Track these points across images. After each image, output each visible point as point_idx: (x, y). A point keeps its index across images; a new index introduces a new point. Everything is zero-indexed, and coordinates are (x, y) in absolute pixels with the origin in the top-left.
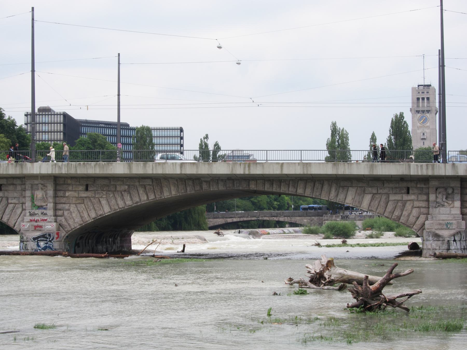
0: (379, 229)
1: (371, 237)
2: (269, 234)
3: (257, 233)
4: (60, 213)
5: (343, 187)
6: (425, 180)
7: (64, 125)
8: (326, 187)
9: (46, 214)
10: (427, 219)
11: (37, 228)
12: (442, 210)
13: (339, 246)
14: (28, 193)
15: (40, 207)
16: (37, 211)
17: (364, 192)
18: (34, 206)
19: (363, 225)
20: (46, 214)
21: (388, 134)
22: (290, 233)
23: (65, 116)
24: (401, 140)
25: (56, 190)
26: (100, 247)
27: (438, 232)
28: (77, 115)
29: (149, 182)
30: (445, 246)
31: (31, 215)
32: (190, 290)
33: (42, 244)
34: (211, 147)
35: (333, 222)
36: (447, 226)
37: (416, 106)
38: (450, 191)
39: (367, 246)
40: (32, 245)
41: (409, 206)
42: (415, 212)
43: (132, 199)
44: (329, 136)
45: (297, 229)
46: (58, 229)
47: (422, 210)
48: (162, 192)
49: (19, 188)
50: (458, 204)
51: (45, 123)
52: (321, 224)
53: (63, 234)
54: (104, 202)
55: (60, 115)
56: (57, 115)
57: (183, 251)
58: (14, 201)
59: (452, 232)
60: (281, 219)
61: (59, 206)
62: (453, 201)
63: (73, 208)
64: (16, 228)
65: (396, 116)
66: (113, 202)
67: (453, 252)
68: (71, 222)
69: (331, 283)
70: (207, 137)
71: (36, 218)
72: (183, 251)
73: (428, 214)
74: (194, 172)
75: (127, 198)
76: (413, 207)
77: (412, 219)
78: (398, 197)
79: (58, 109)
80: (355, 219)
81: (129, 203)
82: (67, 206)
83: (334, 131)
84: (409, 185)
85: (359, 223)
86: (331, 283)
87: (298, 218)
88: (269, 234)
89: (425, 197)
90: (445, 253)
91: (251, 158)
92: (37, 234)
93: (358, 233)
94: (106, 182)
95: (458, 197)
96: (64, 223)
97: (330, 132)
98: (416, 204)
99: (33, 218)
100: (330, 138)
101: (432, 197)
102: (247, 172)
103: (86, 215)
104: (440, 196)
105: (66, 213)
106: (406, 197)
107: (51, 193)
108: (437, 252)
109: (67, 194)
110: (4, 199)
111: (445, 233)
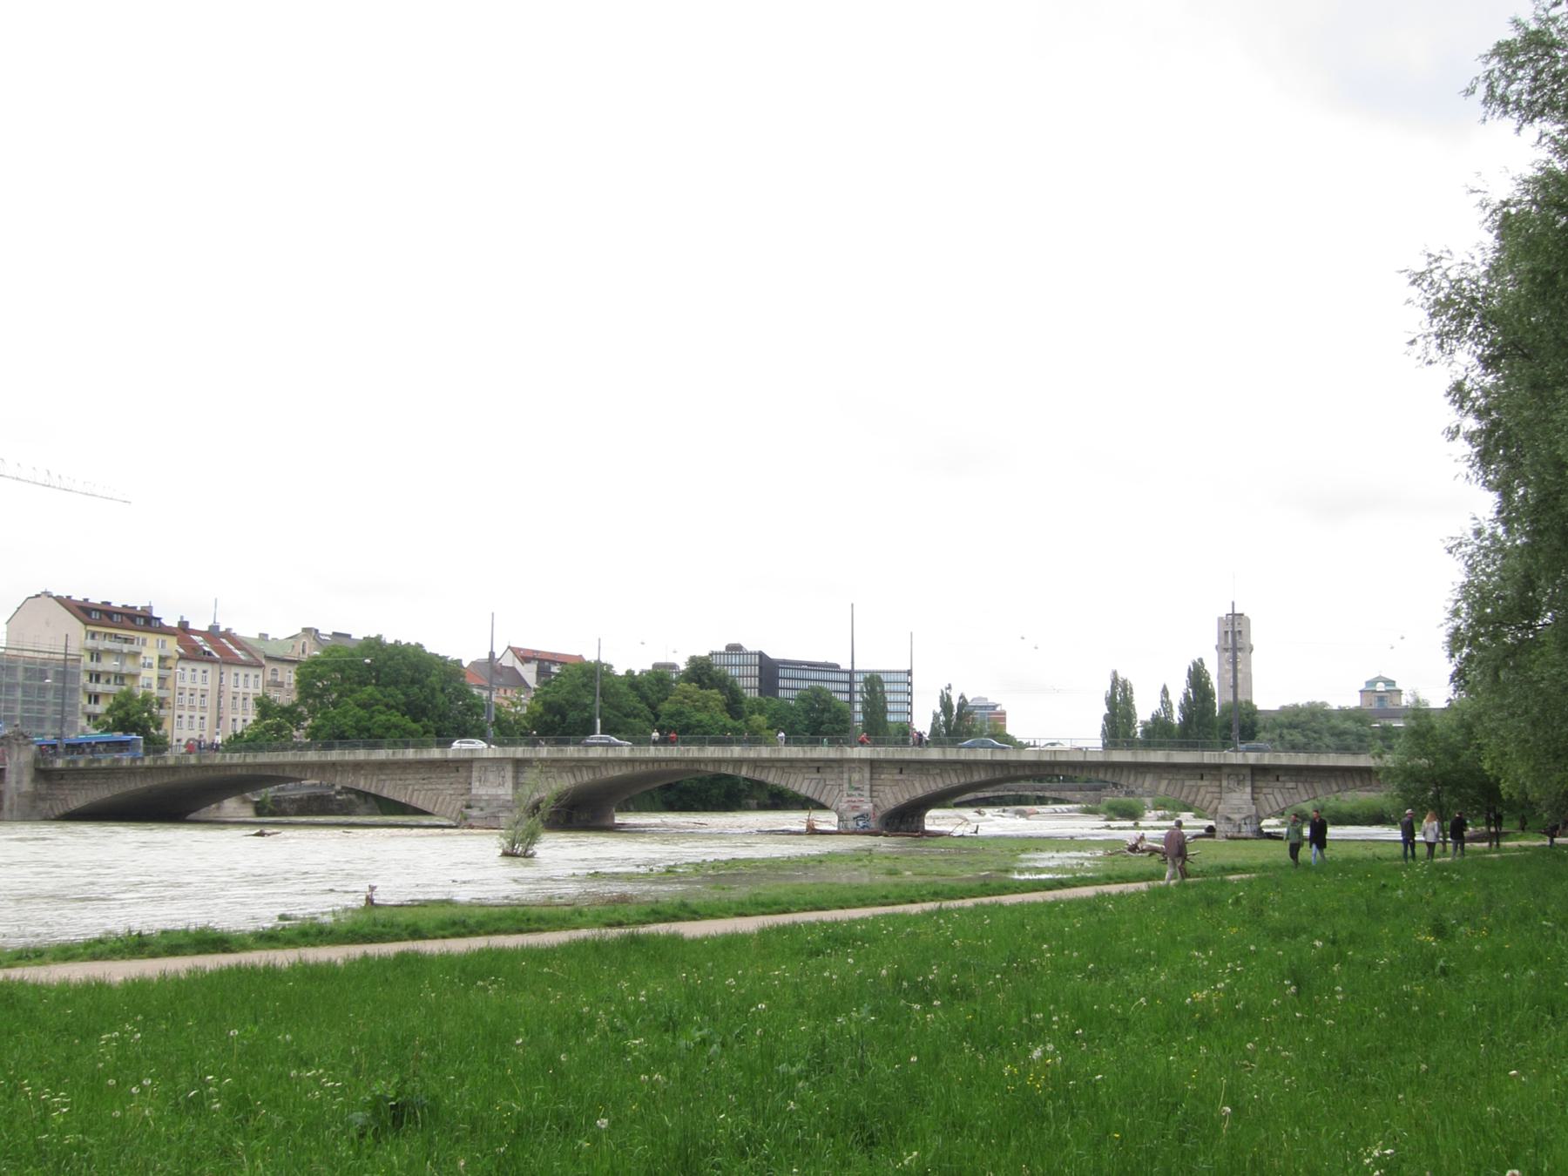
0: (1174, 809)
1: (1163, 818)
2: (1038, 813)
3: (1025, 812)
4: (875, 794)
5: (1141, 773)
6: (1218, 767)
7: (760, 668)
8: (1125, 773)
9: (862, 796)
10: (1220, 803)
11: (855, 808)
12: (1234, 795)
13: (1132, 828)
14: (846, 776)
15: (857, 789)
16: (854, 793)
17: (1161, 778)
18: (851, 787)
19: (1153, 804)
20: (862, 796)
21: (1184, 686)
22: (1063, 812)
23: (761, 655)
24: (1202, 694)
25: (872, 773)
26: (902, 827)
27: (1229, 816)
28: (774, 654)
29: (959, 766)
30: (1236, 829)
31: (848, 796)
32: (843, 911)
33: (861, 823)
34: (955, 702)
35: (1116, 799)
36: (1239, 810)
37: (1223, 642)
38: (1241, 778)
39: (1119, 877)
40: (851, 825)
41: (1202, 791)
42: (1208, 797)
43: (944, 782)
44: (1109, 688)
45: (1064, 807)
46: (874, 810)
47: (1216, 795)
48: (972, 776)
49: (836, 770)
50: (1249, 790)
51: (735, 665)
52: (1099, 802)
53: (879, 814)
54: (917, 785)
55: (755, 654)
56: (751, 654)
57: (976, 832)
58: (832, 783)
59: (1243, 816)
60: (1047, 794)
61: (874, 788)
62: (1244, 787)
63: (887, 789)
64: (828, 805)
65: (1194, 664)
66: (926, 785)
67: (1244, 835)
68: (886, 803)
69: (1143, 851)
70: (949, 687)
71: (853, 799)
72: (976, 832)
73: (1220, 799)
74: (1004, 758)
75: (939, 780)
76: (1207, 792)
77: (1206, 803)
78: (1192, 783)
79: (750, 646)
80: (1142, 795)
81: (941, 785)
82: (881, 788)
83: (1115, 681)
84: (1203, 772)
85: (1148, 801)
86: (1143, 851)
87: (1069, 793)
88: (1038, 813)
89: (1217, 783)
90: (1236, 835)
91: (998, 709)
92: (857, 814)
93: (1147, 814)
94: (919, 766)
95: (1249, 783)
96: (879, 803)
97: (1110, 683)
98: (1210, 789)
99: (849, 799)
100: (1109, 689)
101: (1225, 783)
102: (1053, 759)
103: (900, 797)
104: (1232, 782)
105: (881, 794)
106: (1200, 783)
107: (867, 775)
108: (1229, 835)
109: (883, 777)
110: (822, 781)
111: (1236, 817)
